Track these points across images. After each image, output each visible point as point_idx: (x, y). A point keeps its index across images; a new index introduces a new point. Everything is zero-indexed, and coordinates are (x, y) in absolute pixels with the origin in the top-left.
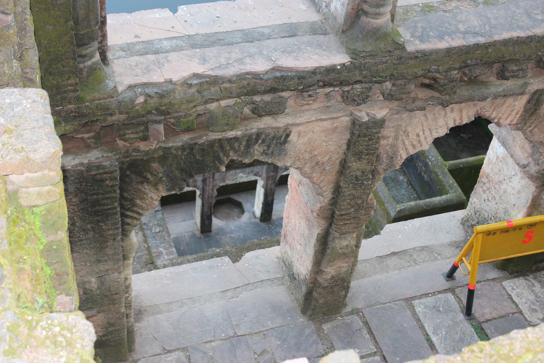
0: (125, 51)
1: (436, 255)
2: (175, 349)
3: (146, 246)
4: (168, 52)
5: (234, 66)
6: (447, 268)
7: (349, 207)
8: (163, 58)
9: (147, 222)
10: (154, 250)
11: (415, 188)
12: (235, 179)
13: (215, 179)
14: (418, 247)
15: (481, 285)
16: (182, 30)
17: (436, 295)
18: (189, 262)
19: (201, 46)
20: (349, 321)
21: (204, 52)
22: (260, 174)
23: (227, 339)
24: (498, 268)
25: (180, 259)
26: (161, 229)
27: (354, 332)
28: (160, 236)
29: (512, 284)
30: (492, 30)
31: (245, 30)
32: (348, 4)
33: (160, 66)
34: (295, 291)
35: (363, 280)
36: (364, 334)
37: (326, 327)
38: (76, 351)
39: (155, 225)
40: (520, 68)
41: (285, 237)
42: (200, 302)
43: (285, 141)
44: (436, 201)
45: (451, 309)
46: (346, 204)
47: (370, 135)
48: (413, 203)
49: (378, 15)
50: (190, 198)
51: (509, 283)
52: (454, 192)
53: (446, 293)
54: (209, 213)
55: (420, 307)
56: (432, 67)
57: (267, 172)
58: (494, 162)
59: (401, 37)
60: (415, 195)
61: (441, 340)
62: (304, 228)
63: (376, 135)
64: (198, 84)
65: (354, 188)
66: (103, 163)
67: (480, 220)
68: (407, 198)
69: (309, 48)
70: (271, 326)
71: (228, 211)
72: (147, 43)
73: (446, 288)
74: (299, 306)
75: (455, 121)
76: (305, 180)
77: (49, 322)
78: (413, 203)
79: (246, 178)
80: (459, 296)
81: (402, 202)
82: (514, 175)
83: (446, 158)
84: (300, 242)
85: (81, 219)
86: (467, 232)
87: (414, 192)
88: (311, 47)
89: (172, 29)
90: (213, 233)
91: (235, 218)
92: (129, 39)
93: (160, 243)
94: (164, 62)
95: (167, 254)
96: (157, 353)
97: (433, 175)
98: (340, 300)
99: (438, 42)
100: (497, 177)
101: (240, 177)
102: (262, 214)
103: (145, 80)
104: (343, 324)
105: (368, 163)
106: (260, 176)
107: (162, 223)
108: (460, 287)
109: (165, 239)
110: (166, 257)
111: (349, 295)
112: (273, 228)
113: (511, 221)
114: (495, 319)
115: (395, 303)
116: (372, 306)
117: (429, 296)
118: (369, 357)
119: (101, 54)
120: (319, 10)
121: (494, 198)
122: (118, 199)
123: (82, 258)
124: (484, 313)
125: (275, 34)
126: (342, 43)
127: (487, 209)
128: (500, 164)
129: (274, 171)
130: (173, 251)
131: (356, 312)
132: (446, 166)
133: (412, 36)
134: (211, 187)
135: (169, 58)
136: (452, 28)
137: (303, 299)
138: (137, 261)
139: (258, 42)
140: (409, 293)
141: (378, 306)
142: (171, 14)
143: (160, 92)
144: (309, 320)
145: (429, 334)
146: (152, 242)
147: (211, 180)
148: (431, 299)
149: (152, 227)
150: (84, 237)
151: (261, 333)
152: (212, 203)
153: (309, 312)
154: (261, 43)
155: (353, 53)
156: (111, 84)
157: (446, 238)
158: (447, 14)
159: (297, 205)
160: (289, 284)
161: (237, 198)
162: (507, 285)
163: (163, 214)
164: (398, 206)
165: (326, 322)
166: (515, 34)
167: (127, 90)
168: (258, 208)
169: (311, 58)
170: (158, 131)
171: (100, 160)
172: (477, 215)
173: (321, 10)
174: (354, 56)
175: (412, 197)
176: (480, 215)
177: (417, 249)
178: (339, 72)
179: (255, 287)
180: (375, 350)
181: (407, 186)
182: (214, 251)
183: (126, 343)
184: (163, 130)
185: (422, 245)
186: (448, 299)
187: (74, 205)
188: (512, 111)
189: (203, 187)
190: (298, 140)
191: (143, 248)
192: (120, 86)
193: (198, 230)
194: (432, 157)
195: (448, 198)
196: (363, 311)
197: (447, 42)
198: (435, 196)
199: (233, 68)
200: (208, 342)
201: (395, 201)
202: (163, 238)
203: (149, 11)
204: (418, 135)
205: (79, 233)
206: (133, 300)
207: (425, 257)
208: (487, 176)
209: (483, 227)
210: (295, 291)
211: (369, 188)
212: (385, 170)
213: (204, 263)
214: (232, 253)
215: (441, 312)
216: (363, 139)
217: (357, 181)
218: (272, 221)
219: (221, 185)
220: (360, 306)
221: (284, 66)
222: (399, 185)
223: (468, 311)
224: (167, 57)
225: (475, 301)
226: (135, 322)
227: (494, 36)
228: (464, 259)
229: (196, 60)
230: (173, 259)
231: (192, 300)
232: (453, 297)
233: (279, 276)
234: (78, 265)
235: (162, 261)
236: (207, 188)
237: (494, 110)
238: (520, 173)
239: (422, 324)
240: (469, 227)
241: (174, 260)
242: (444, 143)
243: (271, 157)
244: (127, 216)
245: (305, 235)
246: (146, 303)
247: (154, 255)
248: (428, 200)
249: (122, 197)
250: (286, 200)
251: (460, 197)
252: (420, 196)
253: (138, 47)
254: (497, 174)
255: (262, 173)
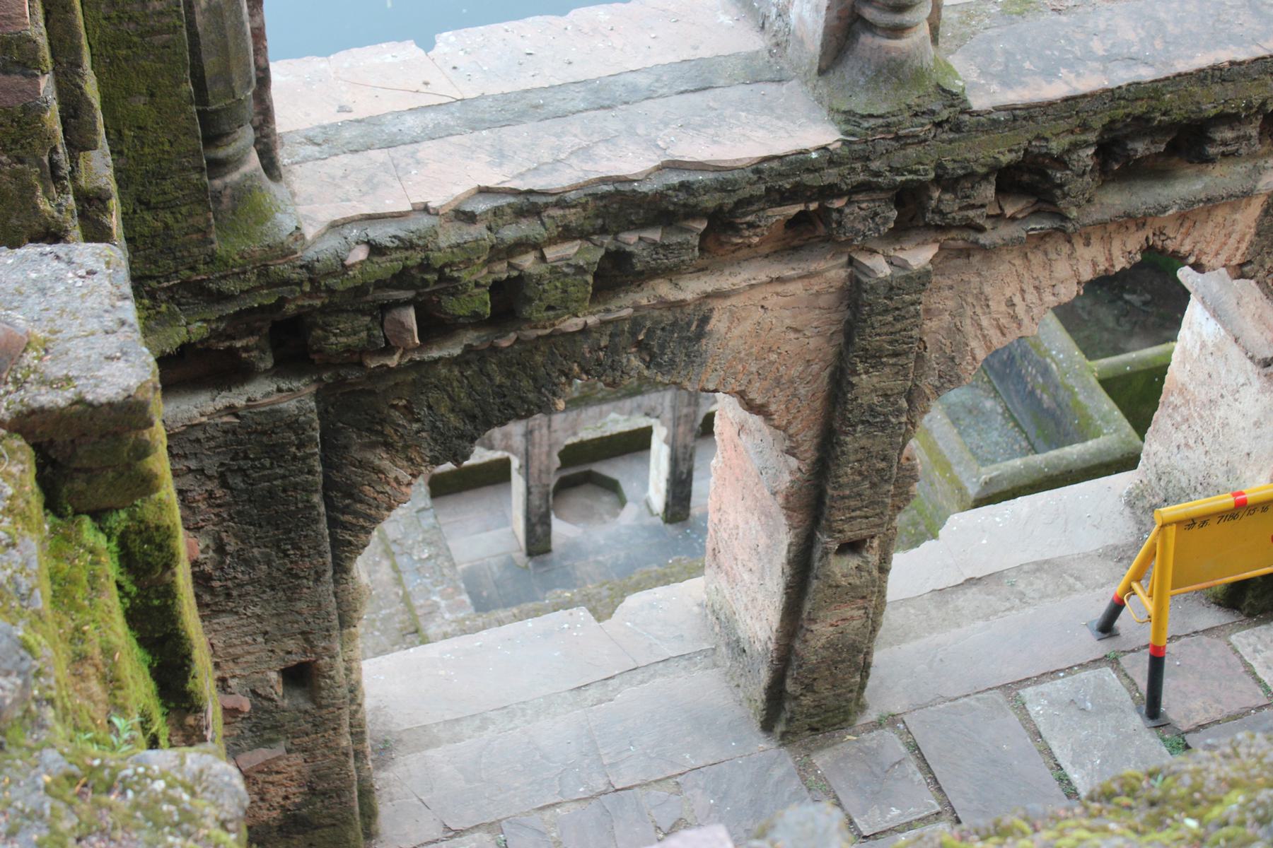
0: (319, 145)
1: (1071, 580)
2: (472, 828)
3: (401, 593)
4: (416, 142)
5: (570, 166)
6: (1100, 609)
7: (858, 478)
8: (405, 156)
9: (399, 537)
10: (418, 602)
11: (1023, 426)
12: (600, 427)
13: (552, 429)
14: (1027, 564)
15: (1181, 645)
16: (447, 88)
17: (1076, 672)
18: (500, 623)
19: (492, 124)
20: (874, 744)
21: (500, 137)
22: (658, 412)
23: (592, 797)
24: (1219, 604)
25: (480, 619)
26: (433, 550)
27: (887, 768)
28: (432, 568)
29: (1253, 639)
30: (1171, 49)
31: (594, 81)
32: (828, 8)
33: (400, 174)
34: (743, 680)
35: (904, 646)
36: (910, 771)
37: (822, 760)
38: (203, 832)
39: (419, 542)
40: (1242, 133)
41: (715, 555)
42: (524, 716)
43: (700, 335)
44: (1072, 454)
45: (1111, 704)
46: (849, 471)
47: (897, 309)
48: (1018, 462)
49: (897, 31)
50: (497, 474)
51: (1246, 637)
52: (1115, 431)
53: (1099, 667)
54: (543, 510)
55: (1037, 703)
56: (1034, 143)
57: (673, 408)
58: (1195, 356)
59: (956, 77)
60: (1024, 444)
61: (1093, 777)
62: (757, 531)
63: (912, 308)
64: (490, 214)
65: (868, 435)
66: (281, 405)
67: (1171, 494)
68: (1005, 451)
69: (743, 114)
70: (694, 763)
71: (588, 502)
72: (369, 123)
73: (1098, 655)
74: (755, 714)
75: (1095, 264)
76: (755, 421)
77: (141, 770)
78: (1018, 462)
79: (627, 424)
80: (1130, 672)
81: (994, 462)
82: (1243, 385)
83: (1091, 351)
84: (751, 565)
85: (236, 536)
86: (1141, 522)
87: (1020, 435)
88: (748, 111)
89: (423, 88)
90: (555, 555)
91: (606, 517)
92: (328, 116)
93: (432, 583)
94: (408, 164)
95: (450, 609)
96: (430, 839)
97: (1062, 394)
98: (850, 695)
99: (1044, 83)
100: (1203, 392)
101: (612, 421)
102: (667, 505)
103: (367, 210)
104: (862, 751)
105: (897, 373)
106: (658, 417)
107: (435, 538)
108: (1129, 652)
109: (443, 575)
110: (447, 616)
111: (870, 683)
112: (695, 536)
113: (1241, 494)
114: (1217, 722)
115: (979, 696)
116: (926, 706)
117: (1060, 678)
118: (925, 825)
119: (261, 154)
120: (763, 24)
121: (1200, 440)
122: (320, 487)
123: (244, 626)
124: (1191, 711)
125: (662, 87)
126: (819, 100)
127: (1186, 466)
128: (1210, 359)
129: (689, 404)
130: (464, 602)
131: (891, 720)
132: (1093, 371)
133: (983, 73)
134: (545, 449)
135: (420, 155)
136: (1077, 50)
137: (764, 697)
138: (382, 628)
139: (624, 107)
140: (1012, 673)
141: (941, 706)
142: (422, 52)
143: (401, 234)
144: (780, 746)
145: (1063, 766)
146: (413, 583)
147: (545, 431)
148: (1063, 683)
149: (412, 548)
150: (247, 577)
151: (670, 781)
152: (548, 485)
153: (780, 728)
154: (632, 108)
155: (847, 122)
156: (288, 221)
157: (1093, 541)
158: (1064, 19)
159: (737, 480)
160: (729, 664)
161: (606, 469)
162: (1240, 642)
163: (436, 517)
164: (983, 470)
165: (821, 748)
166: (1223, 56)
167: (325, 233)
168: (658, 491)
169: (749, 138)
170: (402, 324)
171: (274, 398)
172: (1162, 483)
173: (767, 25)
174: (849, 128)
175: (1016, 447)
176: (1169, 482)
177: (1026, 568)
178: (813, 168)
179: (652, 675)
180: (938, 808)
181: (1004, 422)
182: (560, 597)
183: (358, 819)
184: (414, 322)
185: (1037, 558)
186: (1105, 681)
187: (219, 506)
188: (1229, 235)
189: (527, 451)
190: (729, 328)
191: (393, 597)
192: (310, 225)
193: (521, 550)
194: (1059, 353)
195: (1102, 446)
196: (905, 719)
197: (1066, 83)
198: (1071, 443)
199: (568, 171)
200: (548, 806)
201: (978, 459)
202: (438, 573)
203: (369, 49)
204: (1010, 303)
205: (234, 568)
206: (368, 718)
207: (1045, 587)
208: (1181, 390)
209: (1176, 509)
210: (743, 680)
211: (903, 431)
212: (937, 388)
213: (530, 625)
214: (600, 600)
215: (1089, 712)
216: (880, 318)
217: (875, 417)
218: (691, 519)
219: (570, 441)
220: (897, 709)
221: (686, 159)
222: (984, 422)
223: (1153, 708)
224: (414, 153)
225: (1169, 684)
226: (378, 768)
227: (1176, 63)
228: (1135, 585)
229: (483, 156)
230: (464, 620)
231: (505, 711)
232: (1114, 676)
233: (706, 646)
234: (237, 642)
235: (439, 626)
236: (536, 451)
237: (1187, 234)
238: (1259, 378)
239: (1046, 743)
240: (1145, 511)
241: (467, 623)
242: (1086, 317)
243: (669, 372)
244: (344, 526)
245: (760, 549)
246: (399, 725)
247: (419, 612)
248: (1053, 453)
249: (329, 485)
250: (712, 469)
251: (1130, 443)
252: (1036, 445)
253: (347, 134)
254: (1203, 384)
255: (663, 409)
